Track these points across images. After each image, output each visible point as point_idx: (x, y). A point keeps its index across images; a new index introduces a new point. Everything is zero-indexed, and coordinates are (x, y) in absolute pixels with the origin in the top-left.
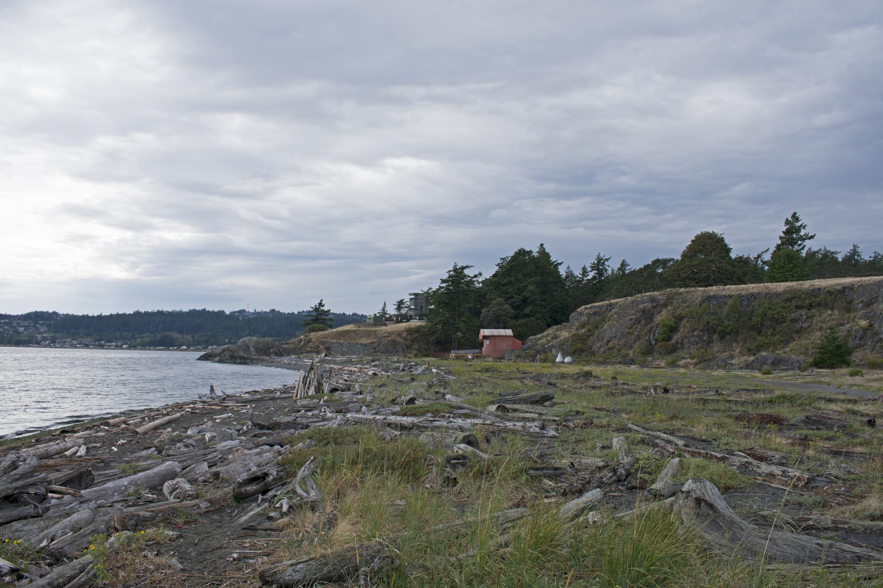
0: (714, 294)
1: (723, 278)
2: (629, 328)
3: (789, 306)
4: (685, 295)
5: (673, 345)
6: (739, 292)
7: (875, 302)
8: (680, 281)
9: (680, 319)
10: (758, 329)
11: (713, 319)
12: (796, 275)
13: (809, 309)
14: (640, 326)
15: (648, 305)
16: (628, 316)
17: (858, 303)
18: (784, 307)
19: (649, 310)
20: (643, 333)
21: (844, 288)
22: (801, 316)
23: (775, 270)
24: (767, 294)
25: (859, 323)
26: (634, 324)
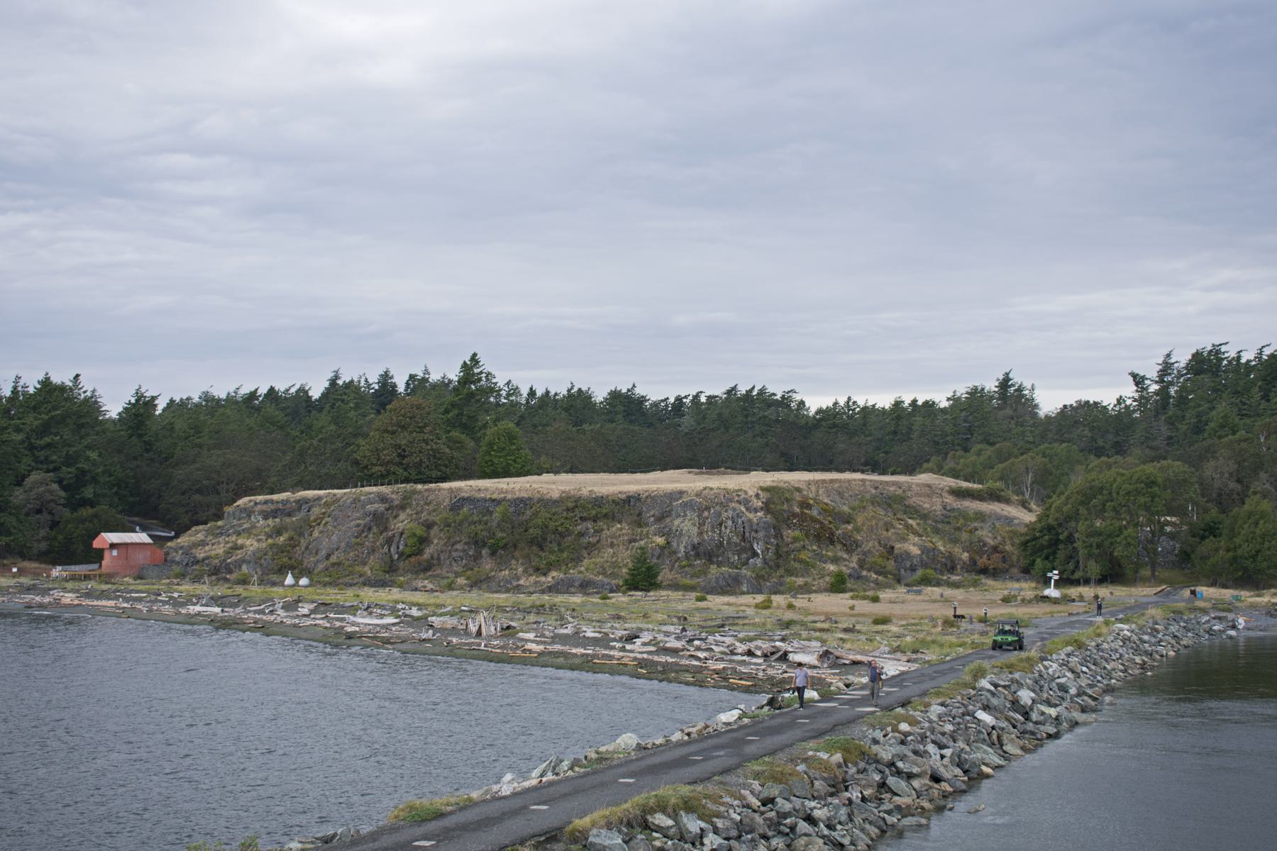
0: (468, 495)
1: (440, 465)
2: (357, 537)
3: (572, 517)
4: (426, 494)
5: (428, 561)
6: (503, 495)
7: (667, 516)
8: (380, 465)
9: (429, 526)
10: (539, 544)
11: (482, 530)
12: (519, 460)
13: (595, 521)
14: (371, 535)
15: (380, 507)
16: (352, 521)
17: (650, 517)
18: (566, 518)
19: (382, 514)
20: (378, 544)
21: (629, 498)
22: (587, 529)
23: (492, 453)
24: (540, 500)
25: (654, 539)
26: (363, 531)
